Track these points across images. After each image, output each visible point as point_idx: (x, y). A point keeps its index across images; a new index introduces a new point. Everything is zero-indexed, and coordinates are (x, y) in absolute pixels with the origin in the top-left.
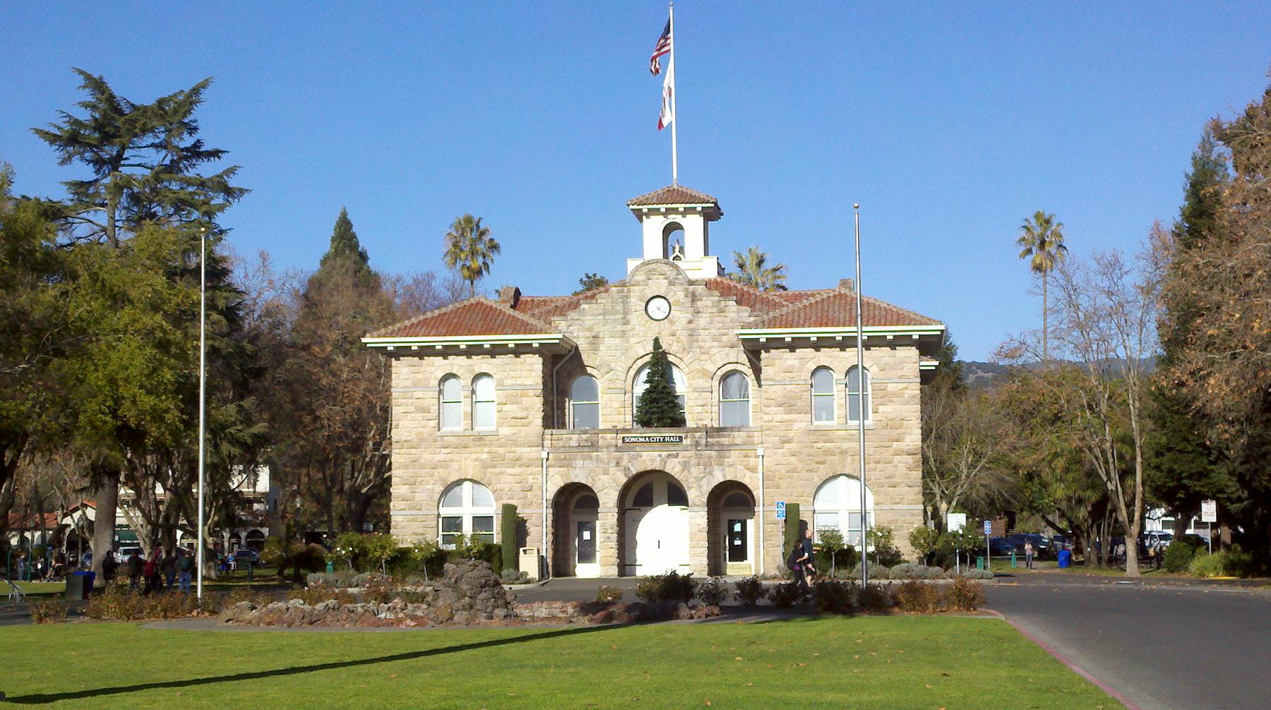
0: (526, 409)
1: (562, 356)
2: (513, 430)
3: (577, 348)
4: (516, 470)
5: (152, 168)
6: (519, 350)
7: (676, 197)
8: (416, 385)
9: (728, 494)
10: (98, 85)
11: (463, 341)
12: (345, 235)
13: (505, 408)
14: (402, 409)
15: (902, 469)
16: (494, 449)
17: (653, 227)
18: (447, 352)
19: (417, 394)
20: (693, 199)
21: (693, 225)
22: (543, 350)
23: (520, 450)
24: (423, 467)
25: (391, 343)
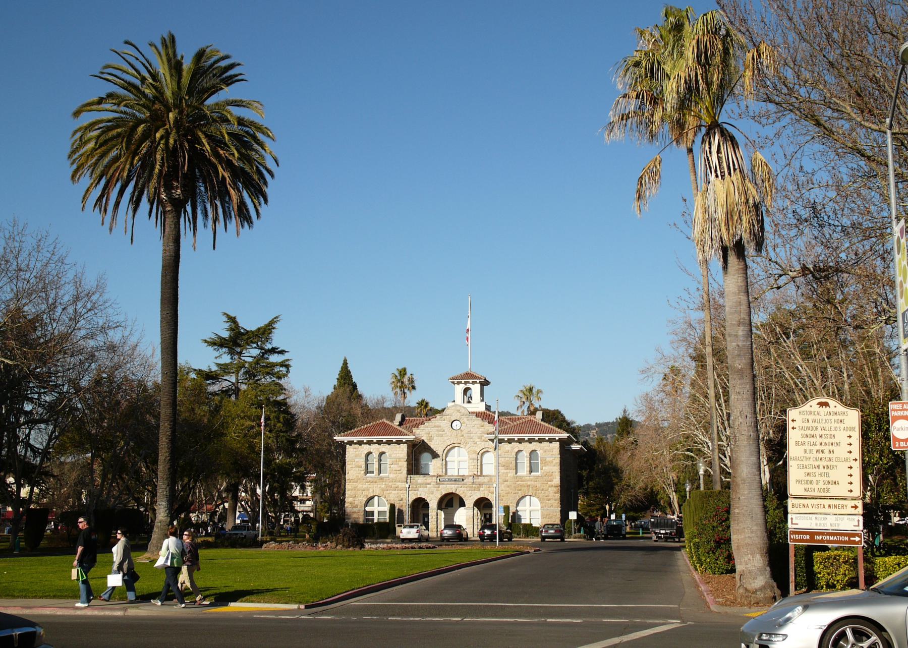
0: (401, 467)
1: (417, 445)
2: (395, 475)
3: (423, 441)
4: (396, 492)
5: (255, 357)
6: (399, 442)
7: (468, 376)
8: (356, 456)
9: (484, 503)
10: (232, 320)
11: (375, 438)
12: (345, 376)
13: (392, 466)
14: (350, 466)
15: (552, 494)
16: (387, 483)
17: (460, 389)
18: (370, 443)
19: (356, 460)
20: (476, 378)
21: (476, 389)
22: (407, 442)
23: (398, 484)
24: (358, 490)
25: (346, 439)
